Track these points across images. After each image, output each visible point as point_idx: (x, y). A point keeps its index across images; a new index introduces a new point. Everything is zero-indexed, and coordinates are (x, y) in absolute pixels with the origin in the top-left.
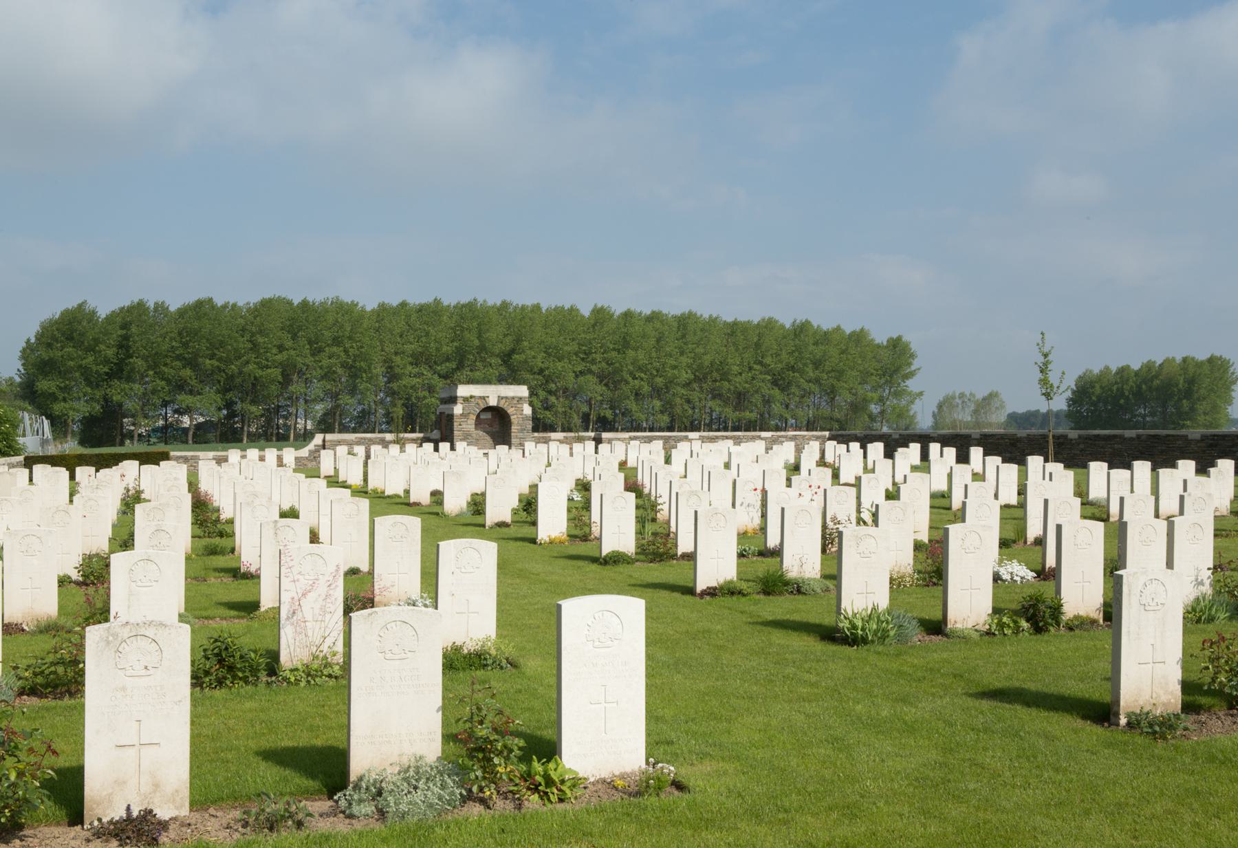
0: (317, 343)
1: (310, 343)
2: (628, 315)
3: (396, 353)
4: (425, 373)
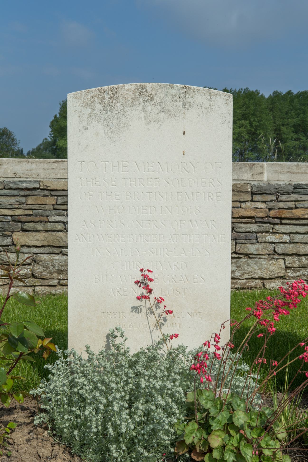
3: (283, 125)
4: (302, 138)
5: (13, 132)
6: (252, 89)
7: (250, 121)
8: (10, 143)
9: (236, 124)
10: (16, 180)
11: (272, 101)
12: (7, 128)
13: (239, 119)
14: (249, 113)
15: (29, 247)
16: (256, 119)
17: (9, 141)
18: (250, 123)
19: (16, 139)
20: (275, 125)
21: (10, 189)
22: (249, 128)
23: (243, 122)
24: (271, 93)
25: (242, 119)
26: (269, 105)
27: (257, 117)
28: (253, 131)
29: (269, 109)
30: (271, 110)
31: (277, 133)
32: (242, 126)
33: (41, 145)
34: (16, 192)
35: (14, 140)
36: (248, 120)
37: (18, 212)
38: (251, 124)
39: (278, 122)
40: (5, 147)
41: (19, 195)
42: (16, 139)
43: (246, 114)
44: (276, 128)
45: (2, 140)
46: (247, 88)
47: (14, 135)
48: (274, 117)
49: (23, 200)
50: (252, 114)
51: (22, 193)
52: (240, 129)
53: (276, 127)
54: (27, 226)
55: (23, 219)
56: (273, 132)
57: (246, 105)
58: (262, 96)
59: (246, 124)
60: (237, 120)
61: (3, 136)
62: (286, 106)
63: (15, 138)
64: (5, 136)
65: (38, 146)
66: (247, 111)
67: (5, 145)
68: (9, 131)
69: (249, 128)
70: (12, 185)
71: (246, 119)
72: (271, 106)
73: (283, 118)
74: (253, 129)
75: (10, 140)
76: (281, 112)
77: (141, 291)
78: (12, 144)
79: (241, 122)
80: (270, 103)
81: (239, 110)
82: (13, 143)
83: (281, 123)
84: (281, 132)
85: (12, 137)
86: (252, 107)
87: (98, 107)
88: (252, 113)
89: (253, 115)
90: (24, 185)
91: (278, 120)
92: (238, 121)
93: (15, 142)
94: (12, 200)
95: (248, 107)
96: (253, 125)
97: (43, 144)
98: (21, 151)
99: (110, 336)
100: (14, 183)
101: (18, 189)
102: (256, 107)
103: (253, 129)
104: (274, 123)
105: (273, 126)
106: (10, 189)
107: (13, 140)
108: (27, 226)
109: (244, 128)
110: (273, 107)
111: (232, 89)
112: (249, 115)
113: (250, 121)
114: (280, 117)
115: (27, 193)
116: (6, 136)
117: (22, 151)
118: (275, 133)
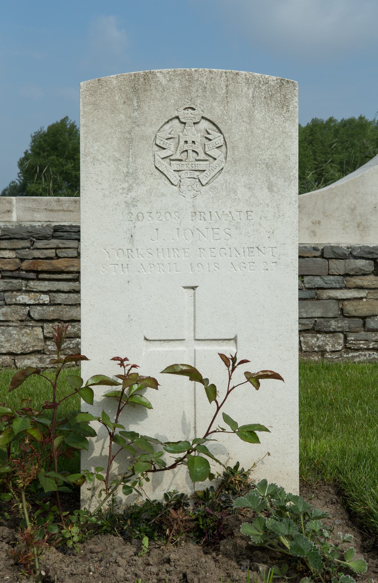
39: (319, 159)
48: (314, 152)
72: (311, 137)
114: (322, 152)
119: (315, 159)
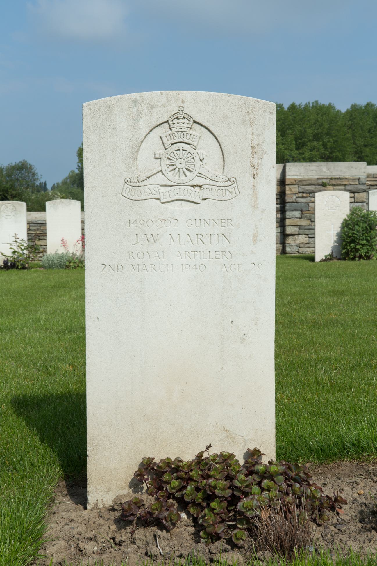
0: (301, 139)
1: (296, 139)
2: (306, 106)
3: (365, 146)
5: (34, 166)
6: (324, 101)
7: (323, 142)
8: (31, 177)
9: (307, 147)
10: (36, 220)
11: (351, 115)
12: (26, 161)
13: (310, 141)
14: (322, 133)
15: (42, 245)
16: (331, 139)
17: (29, 176)
18: (323, 145)
19: (37, 173)
20: (355, 146)
21: (34, 223)
22: (323, 152)
23: (315, 143)
24: (349, 107)
25: (313, 140)
26: (347, 122)
27: (332, 138)
28: (328, 155)
29: (347, 126)
30: (350, 128)
31: (357, 155)
32: (314, 149)
33: (67, 178)
34: (36, 225)
35: (35, 175)
36: (321, 141)
37: (38, 232)
38: (325, 146)
39: (358, 143)
40: (24, 183)
41: (37, 226)
42: (37, 173)
43: (319, 134)
44: (356, 150)
45: (22, 175)
46: (317, 102)
47: (35, 169)
49: (39, 227)
50: (326, 134)
51: (39, 225)
52: (312, 152)
53: (356, 148)
54: (41, 237)
55: (39, 235)
56: (353, 155)
57: (317, 123)
58: (338, 111)
59: (318, 147)
60: (307, 142)
61: (23, 170)
62: (368, 122)
63: (36, 172)
64: (24, 170)
65: (64, 180)
66: (320, 131)
67: (24, 181)
68: (30, 164)
69: (322, 150)
70: (35, 222)
71: (318, 140)
72: (350, 122)
73: (365, 138)
74: (328, 152)
75: (30, 175)
76: (362, 130)
77: (62, 242)
78: (32, 180)
79: (312, 144)
80: (348, 119)
81: (310, 130)
82: (34, 178)
83: (362, 143)
84: (363, 154)
85: (33, 171)
86: (326, 126)
87: (52, 205)
88: (326, 132)
89: (328, 134)
90: (39, 222)
91: (358, 140)
92: (309, 143)
93: (36, 177)
94: (35, 228)
95: (321, 125)
96: (328, 146)
97: (70, 177)
98: (43, 185)
99: (56, 251)
100: (36, 221)
101: (37, 224)
102: (331, 125)
103: (328, 152)
104: (354, 143)
105: (353, 148)
106: (34, 223)
107: (34, 174)
108: (41, 237)
109: (317, 151)
110: (352, 125)
111: (301, 103)
112: (322, 134)
113: (323, 142)
115: (40, 225)
116: (26, 170)
117: (45, 184)
118: (355, 156)
119: (354, 143)
